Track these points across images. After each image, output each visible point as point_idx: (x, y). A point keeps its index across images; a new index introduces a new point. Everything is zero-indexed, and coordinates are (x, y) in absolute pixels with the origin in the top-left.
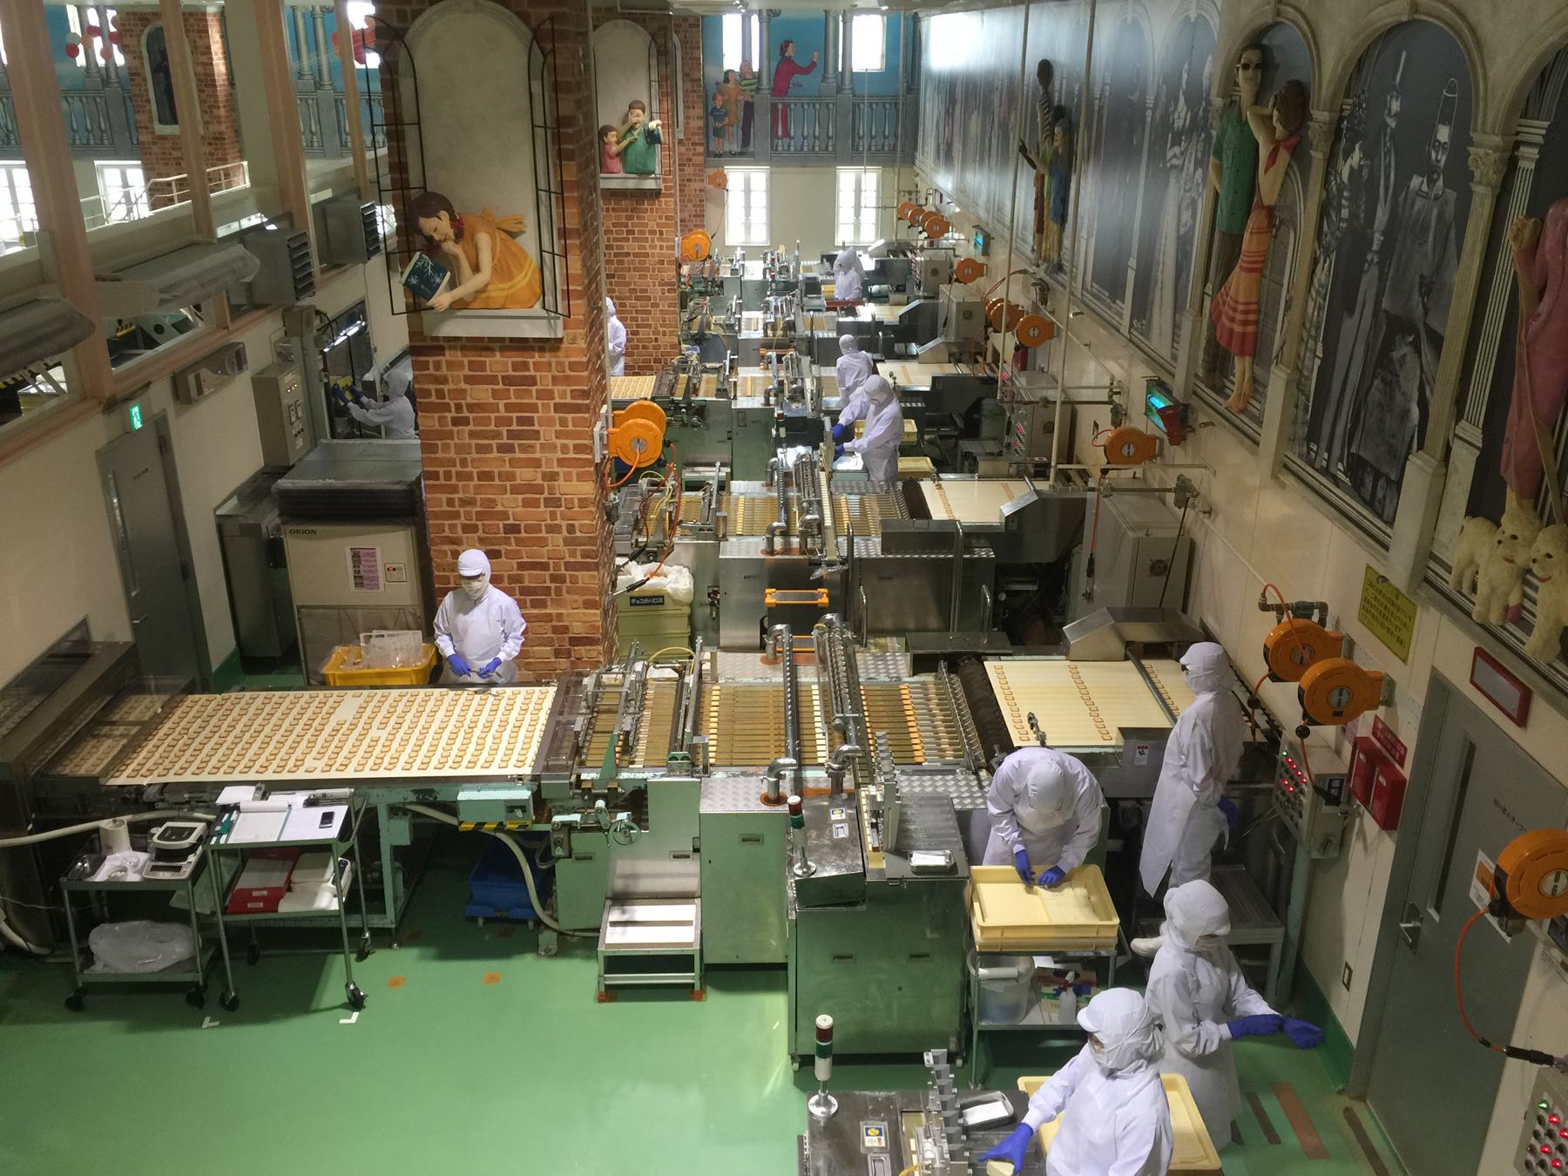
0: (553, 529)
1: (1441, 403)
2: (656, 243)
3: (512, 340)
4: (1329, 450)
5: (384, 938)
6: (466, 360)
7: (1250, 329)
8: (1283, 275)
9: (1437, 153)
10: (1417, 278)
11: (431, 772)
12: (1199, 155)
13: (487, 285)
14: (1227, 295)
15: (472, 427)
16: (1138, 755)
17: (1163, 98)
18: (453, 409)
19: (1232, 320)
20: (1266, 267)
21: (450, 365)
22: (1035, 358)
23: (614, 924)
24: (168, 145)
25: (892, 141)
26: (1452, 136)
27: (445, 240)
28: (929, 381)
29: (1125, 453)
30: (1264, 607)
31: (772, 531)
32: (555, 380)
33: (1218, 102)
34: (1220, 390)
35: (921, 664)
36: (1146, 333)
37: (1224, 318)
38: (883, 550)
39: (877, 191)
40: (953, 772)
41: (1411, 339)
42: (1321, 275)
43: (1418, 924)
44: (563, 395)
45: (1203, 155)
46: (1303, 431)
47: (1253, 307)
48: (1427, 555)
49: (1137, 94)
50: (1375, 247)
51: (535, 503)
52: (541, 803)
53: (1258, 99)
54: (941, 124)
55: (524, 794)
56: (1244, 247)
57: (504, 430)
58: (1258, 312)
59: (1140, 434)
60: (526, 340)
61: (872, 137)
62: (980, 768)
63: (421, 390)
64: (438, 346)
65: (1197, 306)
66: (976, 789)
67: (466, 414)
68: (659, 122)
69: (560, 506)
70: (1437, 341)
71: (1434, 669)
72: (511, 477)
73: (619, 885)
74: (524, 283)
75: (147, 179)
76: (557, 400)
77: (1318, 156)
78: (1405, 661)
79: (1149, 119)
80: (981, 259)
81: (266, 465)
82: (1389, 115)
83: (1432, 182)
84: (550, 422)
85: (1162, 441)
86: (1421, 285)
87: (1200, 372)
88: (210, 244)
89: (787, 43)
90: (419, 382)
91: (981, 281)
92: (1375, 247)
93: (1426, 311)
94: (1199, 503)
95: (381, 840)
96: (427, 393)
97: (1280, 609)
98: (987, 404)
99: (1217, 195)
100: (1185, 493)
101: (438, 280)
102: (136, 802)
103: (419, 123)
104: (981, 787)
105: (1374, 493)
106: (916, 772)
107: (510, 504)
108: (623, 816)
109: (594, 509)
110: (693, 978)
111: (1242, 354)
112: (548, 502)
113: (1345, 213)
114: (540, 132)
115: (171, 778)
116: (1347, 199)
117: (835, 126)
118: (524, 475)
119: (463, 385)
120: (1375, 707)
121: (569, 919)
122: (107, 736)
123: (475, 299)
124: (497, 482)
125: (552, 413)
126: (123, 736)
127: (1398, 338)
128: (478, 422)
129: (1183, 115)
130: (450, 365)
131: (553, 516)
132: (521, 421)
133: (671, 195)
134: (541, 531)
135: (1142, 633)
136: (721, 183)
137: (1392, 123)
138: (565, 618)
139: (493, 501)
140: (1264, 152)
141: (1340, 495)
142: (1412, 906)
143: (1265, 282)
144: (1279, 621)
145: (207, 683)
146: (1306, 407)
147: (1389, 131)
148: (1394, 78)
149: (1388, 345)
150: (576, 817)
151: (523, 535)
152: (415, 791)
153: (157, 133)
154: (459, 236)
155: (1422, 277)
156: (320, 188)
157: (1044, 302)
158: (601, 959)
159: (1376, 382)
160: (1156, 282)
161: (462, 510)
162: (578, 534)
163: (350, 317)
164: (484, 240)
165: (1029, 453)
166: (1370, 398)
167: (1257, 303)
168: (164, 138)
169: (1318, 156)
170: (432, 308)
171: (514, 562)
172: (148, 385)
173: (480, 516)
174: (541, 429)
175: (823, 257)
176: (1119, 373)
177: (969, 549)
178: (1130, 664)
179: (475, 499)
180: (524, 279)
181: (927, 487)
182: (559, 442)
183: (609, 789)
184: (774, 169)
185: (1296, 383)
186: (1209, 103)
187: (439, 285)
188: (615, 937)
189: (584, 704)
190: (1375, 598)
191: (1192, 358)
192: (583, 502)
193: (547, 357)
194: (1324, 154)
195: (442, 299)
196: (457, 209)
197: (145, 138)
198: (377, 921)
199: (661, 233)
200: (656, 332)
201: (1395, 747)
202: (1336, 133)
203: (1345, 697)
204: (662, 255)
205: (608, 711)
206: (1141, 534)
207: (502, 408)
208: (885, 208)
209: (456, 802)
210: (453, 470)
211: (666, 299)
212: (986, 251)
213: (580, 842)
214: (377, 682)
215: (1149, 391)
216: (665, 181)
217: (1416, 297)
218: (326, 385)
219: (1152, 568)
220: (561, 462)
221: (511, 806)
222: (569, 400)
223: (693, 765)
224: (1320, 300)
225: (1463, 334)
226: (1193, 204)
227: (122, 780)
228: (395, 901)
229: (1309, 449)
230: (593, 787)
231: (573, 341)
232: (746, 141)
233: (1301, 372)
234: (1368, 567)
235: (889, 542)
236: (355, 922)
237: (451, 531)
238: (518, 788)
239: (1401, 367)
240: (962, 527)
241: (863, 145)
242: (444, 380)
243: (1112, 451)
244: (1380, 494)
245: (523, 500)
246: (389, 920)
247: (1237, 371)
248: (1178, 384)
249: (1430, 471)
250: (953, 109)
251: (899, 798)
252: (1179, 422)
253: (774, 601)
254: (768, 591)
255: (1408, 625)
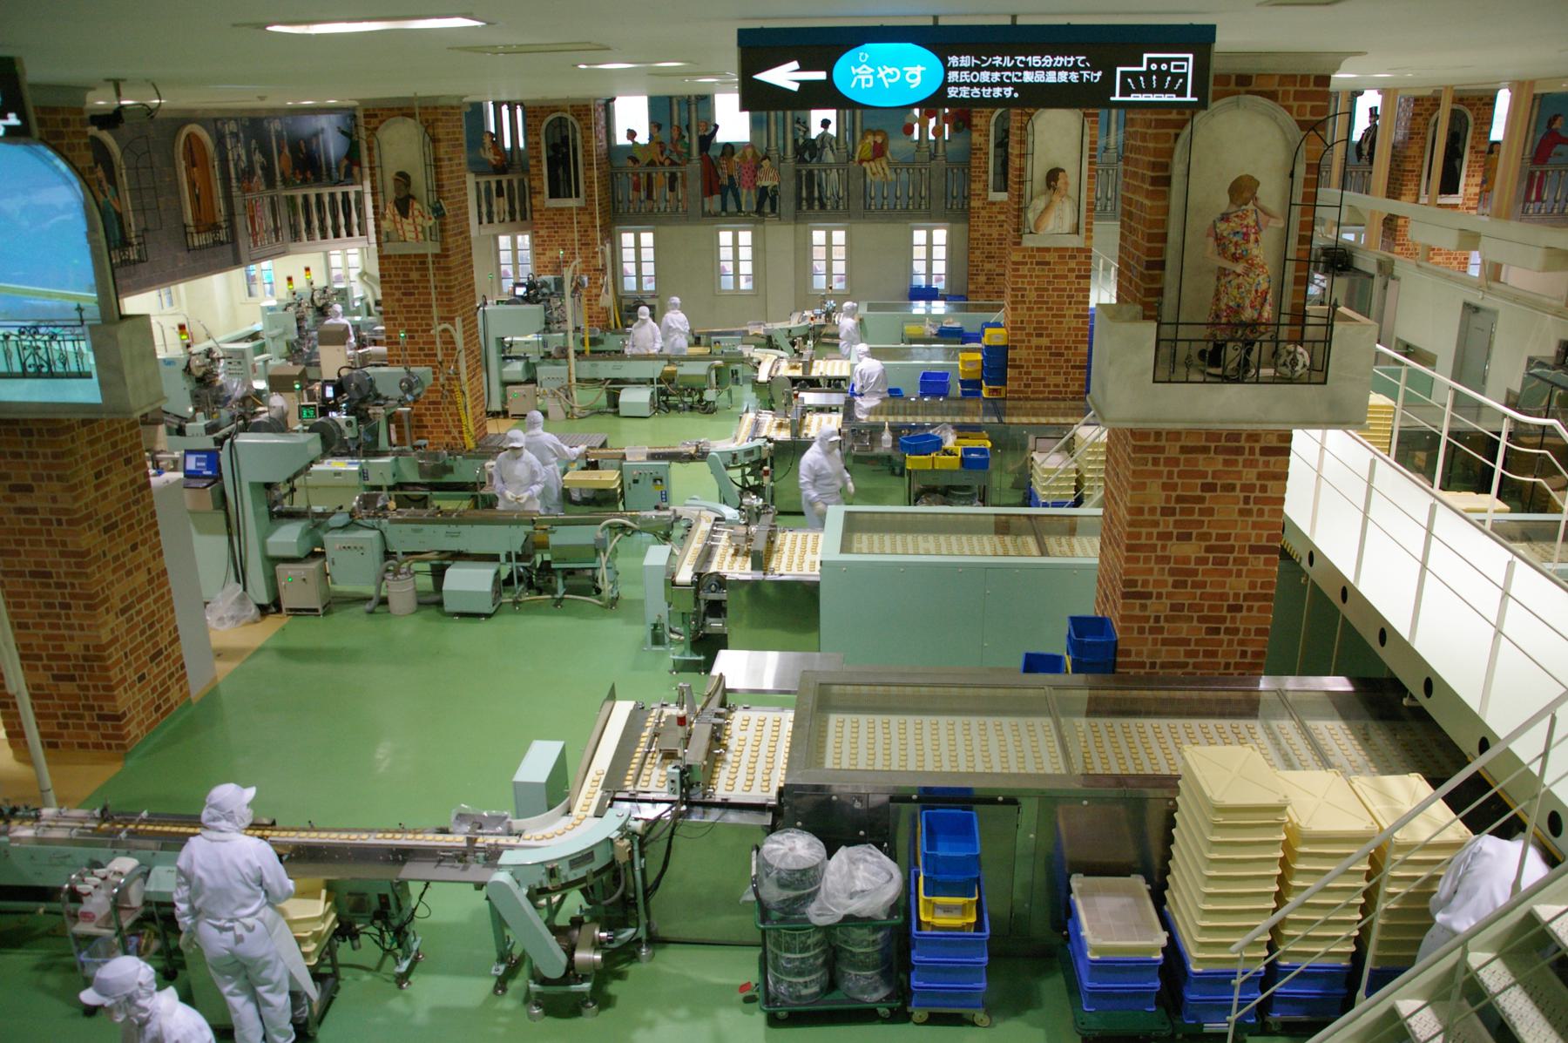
24: (996, 209)
89: (1555, 117)
168: (993, 203)
225: (482, 571)
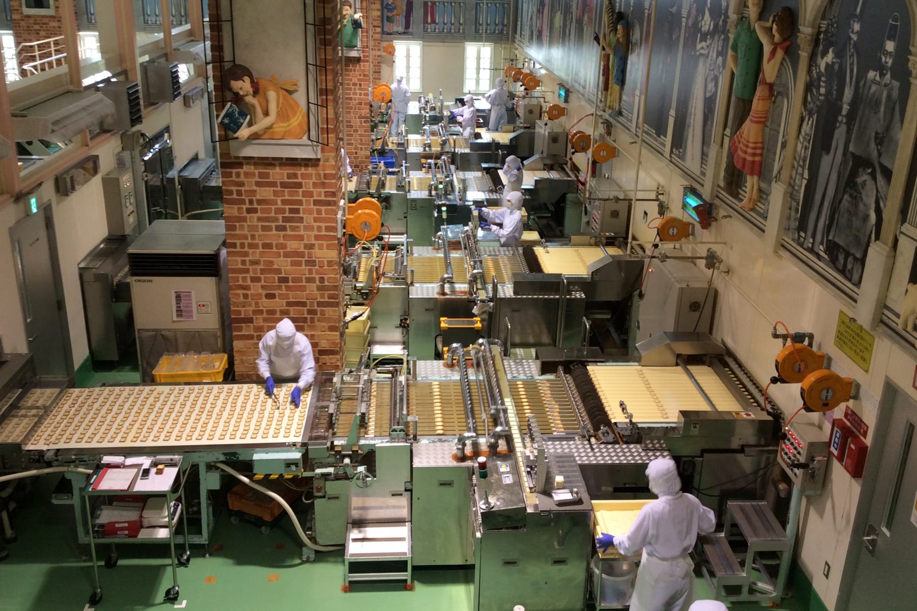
0: (309, 280)
1: (891, 211)
2: (358, 92)
3: (288, 159)
4: (814, 237)
5: (199, 551)
6: (257, 172)
7: (757, 159)
8: (779, 125)
9: (886, 57)
10: (873, 134)
11: (237, 441)
12: (720, 49)
13: (273, 124)
14: (741, 137)
15: (259, 214)
16: (692, 428)
17: (694, 12)
18: (247, 202)
19: (745, 152)
20: (768, 121)
21: (247, 175)
22: (601, 170)
23: (355, 540)
24: (31, 21)
25: (500, 27)
26: (897, 48)
27: (247, 95)
28: (533, 183)
29: (671, 233)
30: (776, 336)
31: (443, 280)
32: (315, 185)
33: (733, 17)
34: (736, 196)
35: (547, 368)
36: (682, 157)
37: (740, 152)
38: (515, 293)
39: (491, 59)
40: (573, 439)
41: (869, 171)
42: (807, 128)
43: (875, 537)
44: (319, 194)
45: (722, 49)
46: (794, 224)
47: (759, 145)
48: (883, 306)
49: (675, 8)
50: (844, 112)
51: (299, 264)
52: (307, 461)
53: (761, 17)
54: (534, 18)
55: (297, 455)
56: (754, 107)
57: (280, 216)
58: (762, 148)
59: (680, 221)
60: (296, 159)
61: (487, 25)
62: (590, 436)
63: (227, 190)
64: (239, 163)
65: (719, 141)
66: (589, 450)
67: (255, 206)
68: (361, 14)
69: (315, 266)
70: (888, 174)
71: (887, 377)
72: (283, 246)
73: (355, 514)
74: (296, 123)
75: (18, 44)
76: (316, 198)
77: (804, 55)
78: (867, 371)
79: (684, 24)
80: (563, 105)
81: (109, 234)
82: (852, 32)
83: (882, 75)
84: (310, 212)
85: (693, 226)
86: (876, 138)
87: (722, 184)
88: (80, 92)
90: (225, 186)
91: (563, 119)
92: (844, 112)
93: (880, 154)
94: (722, 267)
95: (201, 486)
96: (231, 193)
97: (785, 337)
98: (570, 197)
99: (733, 74)
100: (712, 260)
101: (242, 121)
102: (38, 461)
103: (231, 21)
104: (592, 449)
105: (845, 265)
106: (550, 439)
107: (283, 264)
108: (361, 469)
109: (336, 267)
110: (407, 576)
111: (752, 174)
112: (308, 263)
113: (823, 90)
114: (310, 28)
115: (62, 445)
116: (824, 82)
117: (464, 17)
118: (292, 245)
119: (255, 188)
120: (847, 400)
121: (325, 538)
122: (25, 416)
123: (265, 133)
124: (274, 250)
125: (312, 206)
126: (34, 416)
127: (860, 170)
128: (263, 211)
129: (708, 23)
130: (247, 175)
131: (310, 272)
132: (292, 211)
133: (367, 61)
134: (302, 281)
135: (686, 349)
136: (391, 51)
137: (854, 37)
138: (316, 338)
139: (272, 263)
140: (767, 49)
141: (821, 266)
142: (871, 526)
143: (767, 130)
144: (784, 345)
145: (74, 381)
146: (797, 210)
147: (852, 42)
148: (856, 10)
149: (854, 174)
150: (331, 470)
151: (291, 284)
152: (225, 454)
153: (25, 13)
154: (256, 92)
155: (877, 133)
156: (142, 55)
157: (609, 134)
158: (347, 563)
159: (846, 197)
160: (689, 126)
161: (251, 268)
162: (326, 283)
163: (158, 137)
164: (272, 95)
165: (602, 230)
166: (842, 205)
167: (762, 143)
168: (29, 17)
169: (804, 55)
170: (237, 138)
171: (284, 302)
172: (40, 184)
173: (263, 271)
174: (305, 216)
175: (457, 100)
176: (662, 181)
177: (569, 293)
178: (679, 368)
179: (260, 260)
180: (297, 120)
181: (539, 251)
182: (316, 225)
183: (353, 451)
184: (425, 44)
185: (791, 194)
186: (727, 17)
187: (242, 124)
188: (355, 549)
189: (334, 394)
190: (846, 332)
191: (716, 176)
192: (330, 263)
193: (310, 170)
194: (808, 54)
195: (244, 132)
196: (255, 75)
197: (15, 16)
198: (196, 540)
199: (360, 85)
200: (356, 148)
201: (860, 426)
202: (816, 42)
203: (830, 394)
204: (359, 99)
205: (350, 399)
206: (684, 285)
207: (279, 202)
208: (496, 69)
209: (252, 461)
210: (246, 242)
211: (363, 127)
212: (566, 101)
213: (331, 487)
214: (197, 380)
215: (685, 195)
216: (363, 52)
217: (873, 145)
218: (146, 182)
219: (691, 307)
220: (317, 237)
221: (289, 464)
222: (323, 198)
223: (407, 435)
224: (806, 143)
226: (716, 79)
227: (30, 447)
228: (208, 525)
229: (799, 236)
230: (343, 450)
231: (327, 160)
232: (407, 26)
233: (793, 187)
234: (841, 312)
235: (518, 287)
236: (180, 540)
237: (243, 281)
238: (294, 451)
239: (863, 188)
240: (567, 278)
241: (482, 29)
242: (242, 184)
243: (663, 233)
244: (849, 266)
245: (291, 261)
246: (203, 539)
247: (748, 184)
248: (706, 192)
249: (885, 254)
250: (543, 9)
251: (546, 458)
252: (706, 214)
253: (446, 325)
254: (442, 319)
255: (869, 349)
